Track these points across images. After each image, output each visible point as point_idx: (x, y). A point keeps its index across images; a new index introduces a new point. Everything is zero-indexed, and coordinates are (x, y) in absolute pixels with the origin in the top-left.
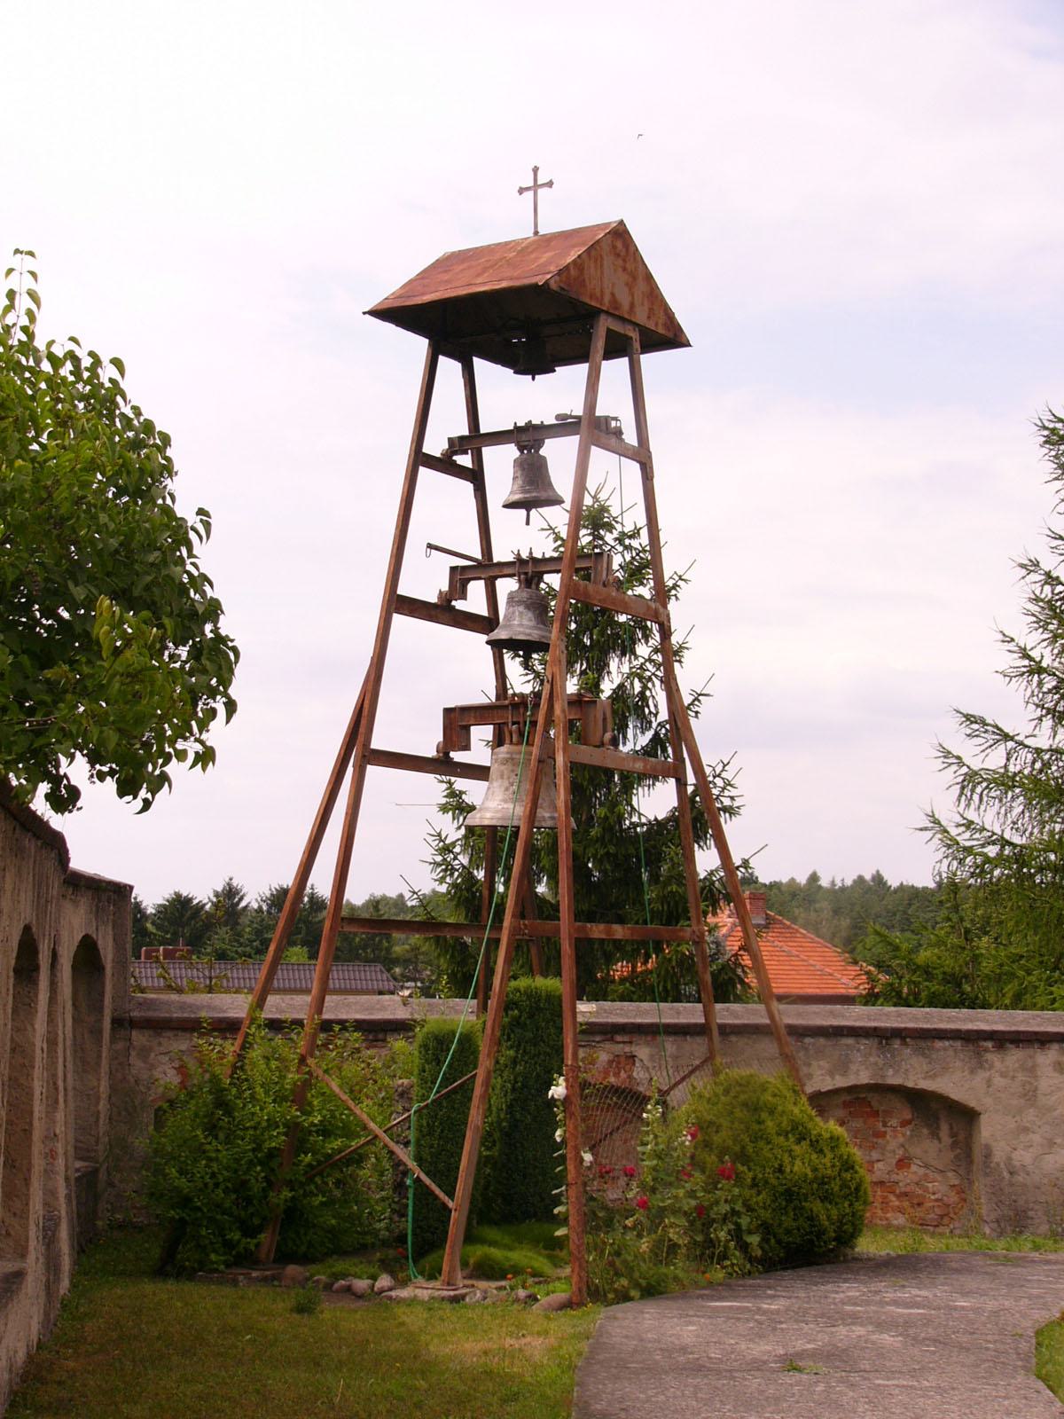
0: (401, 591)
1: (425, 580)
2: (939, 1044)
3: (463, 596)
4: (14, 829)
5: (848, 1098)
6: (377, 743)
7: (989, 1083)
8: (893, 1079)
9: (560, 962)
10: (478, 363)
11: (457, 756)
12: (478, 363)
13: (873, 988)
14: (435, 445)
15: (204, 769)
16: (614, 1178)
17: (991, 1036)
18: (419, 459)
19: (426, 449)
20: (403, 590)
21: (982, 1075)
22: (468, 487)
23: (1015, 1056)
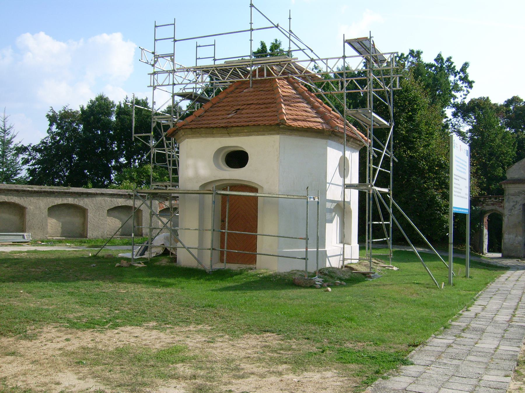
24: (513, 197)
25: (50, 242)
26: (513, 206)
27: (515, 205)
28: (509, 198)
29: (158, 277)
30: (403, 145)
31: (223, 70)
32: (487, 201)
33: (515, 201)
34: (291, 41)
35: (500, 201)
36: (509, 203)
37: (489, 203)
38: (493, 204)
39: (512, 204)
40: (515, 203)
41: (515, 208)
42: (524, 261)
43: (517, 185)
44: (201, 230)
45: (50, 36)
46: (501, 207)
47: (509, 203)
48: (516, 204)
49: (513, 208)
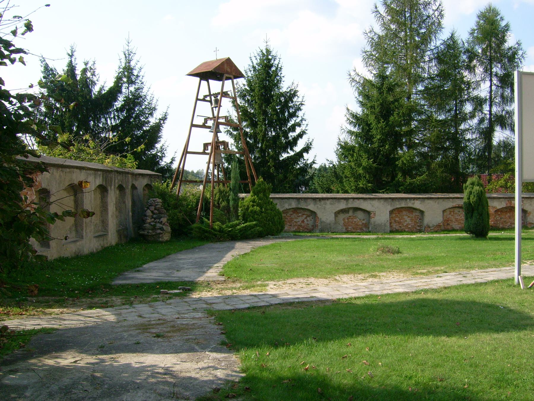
0: (193, 123)
1: (199, 121)
2: (308, 200)
3: (207, 123)
4: (336, 280)
5: (292, 210)
6: (188, 150)
7: (318, 207)
8: (300, 206)
9: (242, 309)
10: (210, 81)
11: (207, 151)
12: (210, 81)
13: (312, 181)
14: (201, 97)
15: (48, 71)
16: (522, 55)
17: (318, 198)
18: (197, 99)
19: (199, 98)
20: (194, 123)
21: (316, 206)
22: (210, 103)
23: (323, 202)
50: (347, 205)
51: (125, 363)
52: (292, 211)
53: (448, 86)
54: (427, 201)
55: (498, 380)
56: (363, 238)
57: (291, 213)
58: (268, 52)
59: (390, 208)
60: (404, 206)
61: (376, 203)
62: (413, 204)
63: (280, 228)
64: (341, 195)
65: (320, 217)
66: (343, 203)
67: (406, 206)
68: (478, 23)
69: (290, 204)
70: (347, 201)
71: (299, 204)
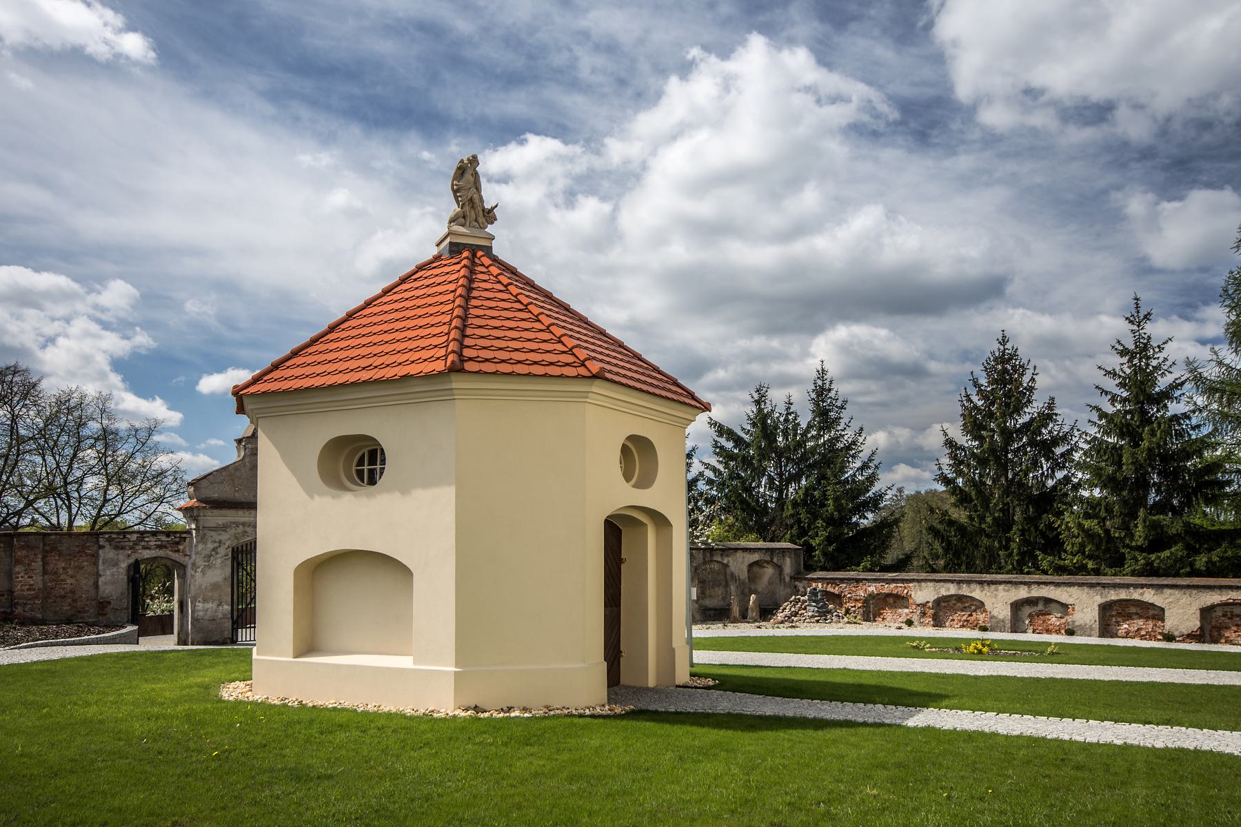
23: (993, 587)
24: (213, 533)
25: (193, 612)
26: (214, 550)
27: (217, 548)
28: (205, 535)
29: (1222, 530)
30: (48, 434)
31: (692, 580)
32: (146, 539)
33: (217, 540)
34: (591, 375)
35: (177, 540)
36: (205, 543)
37: (152, 543)
38: (160, 547)
39: (210, 546)
40: (218, 544)
41: (217, 553)
42: (2, 610)
43: (224, 512)
44: (128, 602)
45: (48, 272)
46: (178, 551)
47: (205, 543)
48: (220, 546)
49: (213, 553)
50: (1029, 593)
51: (1229, 651)
52: (956, 600)
53: (1134, 460)
54: (1168, 591)
55: (1222, 382)
56: (1142, 638)
57: (955, 602)
58: (111, 356)
59: (1099, 600)
60: (1125, 598)
61: (1074, 591)
62: (1142, 594)
63: (1027, 610)
64: (1036, 577)
65: (988, 610)
66: (1024, 589)
67: (1128, 598)
68: (148, 42)
69: (949, 589)
70: (1029, 587)
71: (959, 589)
